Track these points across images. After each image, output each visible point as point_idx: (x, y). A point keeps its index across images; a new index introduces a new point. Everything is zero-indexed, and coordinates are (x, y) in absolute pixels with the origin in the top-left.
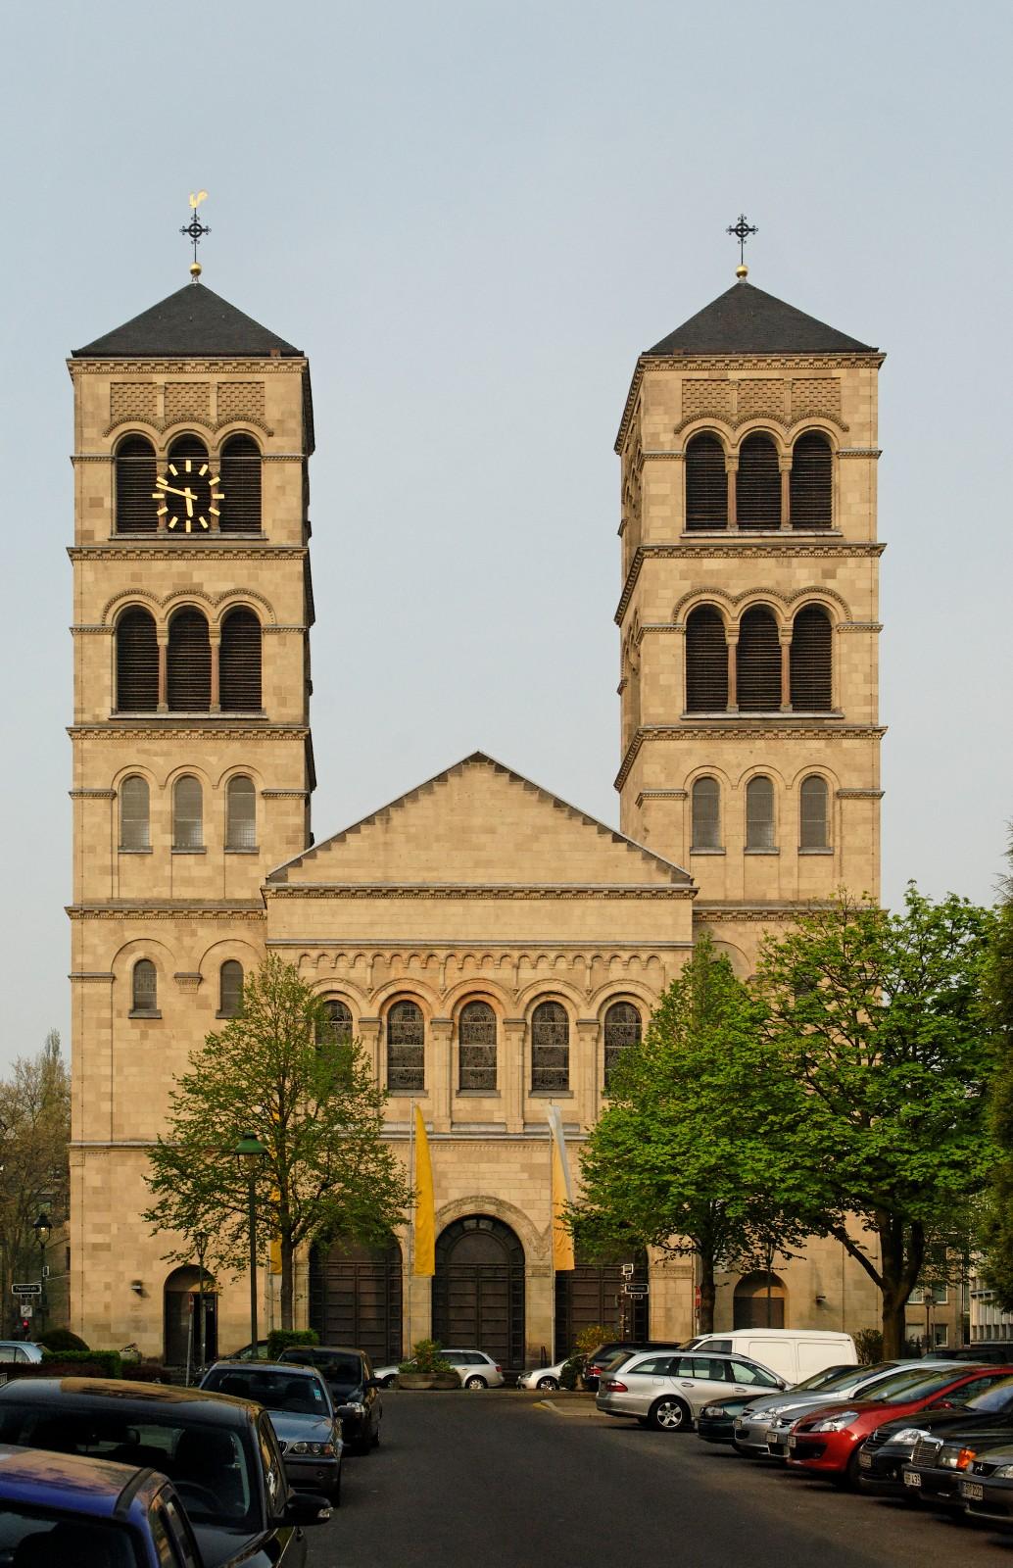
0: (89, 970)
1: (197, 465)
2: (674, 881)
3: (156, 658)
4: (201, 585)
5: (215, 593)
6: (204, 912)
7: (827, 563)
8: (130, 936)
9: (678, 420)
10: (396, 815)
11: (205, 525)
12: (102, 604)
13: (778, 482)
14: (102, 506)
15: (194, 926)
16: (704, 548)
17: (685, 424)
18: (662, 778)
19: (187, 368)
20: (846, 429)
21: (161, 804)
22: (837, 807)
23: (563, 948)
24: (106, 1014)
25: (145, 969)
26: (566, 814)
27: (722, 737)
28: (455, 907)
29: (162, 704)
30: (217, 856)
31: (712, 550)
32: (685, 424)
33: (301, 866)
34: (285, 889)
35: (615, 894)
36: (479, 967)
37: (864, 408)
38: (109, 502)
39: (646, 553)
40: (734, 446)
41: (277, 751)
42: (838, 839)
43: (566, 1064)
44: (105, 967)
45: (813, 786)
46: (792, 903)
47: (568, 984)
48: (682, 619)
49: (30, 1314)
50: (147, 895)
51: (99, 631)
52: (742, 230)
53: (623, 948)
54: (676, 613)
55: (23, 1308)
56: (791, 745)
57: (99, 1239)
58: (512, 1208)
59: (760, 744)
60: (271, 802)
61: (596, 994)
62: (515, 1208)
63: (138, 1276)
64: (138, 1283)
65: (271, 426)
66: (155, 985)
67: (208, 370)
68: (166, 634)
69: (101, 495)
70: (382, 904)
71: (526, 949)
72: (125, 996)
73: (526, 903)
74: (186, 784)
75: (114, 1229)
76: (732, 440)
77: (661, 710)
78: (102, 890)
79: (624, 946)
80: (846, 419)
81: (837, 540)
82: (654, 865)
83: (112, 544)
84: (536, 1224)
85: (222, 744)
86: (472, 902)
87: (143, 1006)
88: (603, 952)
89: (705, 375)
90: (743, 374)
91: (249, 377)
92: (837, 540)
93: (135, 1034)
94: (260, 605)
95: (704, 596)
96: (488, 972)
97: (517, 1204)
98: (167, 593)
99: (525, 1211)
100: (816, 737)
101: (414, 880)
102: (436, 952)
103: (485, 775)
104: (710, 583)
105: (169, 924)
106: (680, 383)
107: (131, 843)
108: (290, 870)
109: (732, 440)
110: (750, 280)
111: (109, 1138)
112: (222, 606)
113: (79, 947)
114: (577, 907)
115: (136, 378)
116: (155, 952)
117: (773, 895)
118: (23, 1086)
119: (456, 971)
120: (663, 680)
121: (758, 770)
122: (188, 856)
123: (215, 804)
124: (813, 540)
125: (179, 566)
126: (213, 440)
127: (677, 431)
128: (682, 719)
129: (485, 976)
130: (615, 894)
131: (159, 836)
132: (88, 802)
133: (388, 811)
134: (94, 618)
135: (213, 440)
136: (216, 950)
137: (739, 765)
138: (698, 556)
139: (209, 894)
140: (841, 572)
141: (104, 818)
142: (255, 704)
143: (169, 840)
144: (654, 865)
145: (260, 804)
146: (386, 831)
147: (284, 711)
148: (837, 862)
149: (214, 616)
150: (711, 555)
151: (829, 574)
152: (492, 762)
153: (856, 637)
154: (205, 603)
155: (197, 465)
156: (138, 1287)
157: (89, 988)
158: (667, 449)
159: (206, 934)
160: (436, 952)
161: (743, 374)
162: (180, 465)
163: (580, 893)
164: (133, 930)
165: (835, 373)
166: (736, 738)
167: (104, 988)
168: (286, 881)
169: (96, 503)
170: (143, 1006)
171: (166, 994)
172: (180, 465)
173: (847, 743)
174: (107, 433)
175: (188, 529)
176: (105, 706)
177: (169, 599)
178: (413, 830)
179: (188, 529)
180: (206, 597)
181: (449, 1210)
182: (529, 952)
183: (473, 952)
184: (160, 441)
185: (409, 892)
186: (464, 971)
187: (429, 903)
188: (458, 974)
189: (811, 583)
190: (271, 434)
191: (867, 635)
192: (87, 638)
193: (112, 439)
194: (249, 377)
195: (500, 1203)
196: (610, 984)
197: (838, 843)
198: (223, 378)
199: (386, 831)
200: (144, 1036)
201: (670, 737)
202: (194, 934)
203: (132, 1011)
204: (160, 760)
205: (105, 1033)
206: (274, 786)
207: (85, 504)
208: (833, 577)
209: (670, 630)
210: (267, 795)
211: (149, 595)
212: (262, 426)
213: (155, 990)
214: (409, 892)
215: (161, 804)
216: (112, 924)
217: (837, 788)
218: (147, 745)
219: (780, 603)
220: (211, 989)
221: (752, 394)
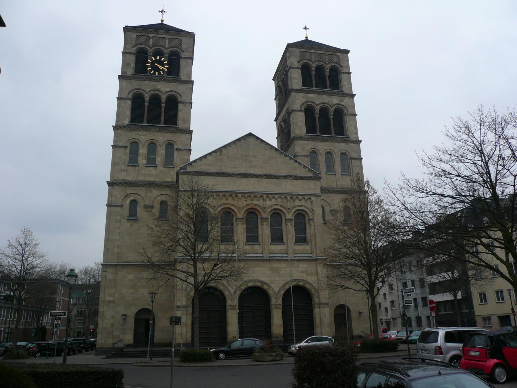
0: (113, 203)
1: (160, 58)
2: (313, 175)
3: (144, 109)
4: (160, 88)
5: (164, 91)
6: (155, 185)
7: (341, 98)
8: (129, 192)
9: (298, 60)
10: (224, 151)
11: (162, 73)
12: (128, 91)
13: (325, 77)
14: (130, 65)
15: (151, 189)
16: (308, 91)
17: (300, 61)
18: (301, 151)
19: (159, 33)
20: (342, 67)
21: (143, 151)
22: (350, 162)
23: (280, 195)
24: (118, 218)
25: (134, 203)
26: (279, 153)
27: (317, 141)
28: (244, 180)
29: (145, 121)
30: (160, 168)
31: (310, 91)
32: (300, 61)
33: (191, 165)
34: (186, 172)
35: (296, 178)
36: (252, 200)
37: (346, 62)
38: (133, 65)
39: (292, 91)
40: (313, 68)
41: (182, 137)
42: (351, 171)
43: (282, 234)
44: (119, 202)
45: (344, 154)
46: (341, 188)
47: (282, 206)
48: (303, 109)
49: (93, 328)
50: (136, 179)
51: (127, 99)
52: (306, 29)
53: (299, 195)
54: (301, 106)
55: (91, 326)
56: (336, 144)
57: (111, 299)
58: (266, 283)
59: (328, 143)
60: (179, 152)
61: (291, 209)
62: (267, 284)
63: (125, 313)
64: (125, 315)
65: (183, 50)
66: (137, 209)
67: (165, 34)
68: (148, 102)
69: (130, 63)
70: (219, 178)
71: (269, 195)
72: (126, 211)
73: (267, 180)
74: (152, 146)
75: (117, 295)
76: (314, 65)
77: (299, 132)
78: (122, 177)
79: (300, 194)
80: (342, 64)
81: (343, 93)
82: (307, 170)
83: (133, 76)
84: (274, 289)
85: (164, 134)
86: (250, 179)
87: (133, 214)
88: (293, 196)
89: (305, 50)
90: (315, 51)
91: (177, 37)
92: (343, 93)
93: (128, 225)
94: (178, 95)
95: (309, 103)
96: (255, 202)
97: (268, 282)
98: (149, 90)
99: (271, 285)
100: (343, 142)
101: (230, 171)
102: (238, 194)
103: (253, 140)
104: (310, 100)
105: (143, 189)
106: (299, 51)
107: (133, 160)
108: (188, 166)
109: (314, 65)
110: (309, 39)
111: (116, 261)
112: (166, 95)
113: (110, 195)
114: (284, 182)
115: (144, 34)
116: (138, 198)
117: (335, 186)
118: (96, 268)
119: (245, 201)
120: (299, 124)
121: (328, 150)
122: (150, 167)
123: (161, 152)
124: (337, 92)
125: (153, 83)
126: (167, 52)
127: (298, 62)
128: (305, 135)
129: (255, 203)
130: (296, 178)
131: (142, 161)
132: (118, 149)
133: (221, 152)
134: (125, 95)
135: (167, 52)
136: (159, 197)
137: (322, 149)
138: (306, 93)
139: (158, 180)
140: (345, 100)
141: (125, 154)
142: (176, 123)
143: (145, 162)
144: (307, 170)
145: (175, 153)
146: (221, 155)
147: (184, 125)
148: (352, 177)
149: (164, 98)
150: (310, 93)
151: (342, 101)
152: (255, 136)
153: (351, 117)
154: (161, 94)
155: (160, 58)
156: (125, 317)
157: (113, 209)
158: (296, 66)
159: (155, 192)
160: (238, 194)
161: (315, 51)
162: (156, 58)
163: (285, 177)
164: (130, 190)
165: (338, 54)
166: (321, 141)
167: (119, 209)
168: (186, 169)
169: (129, 64)
170: (133, 214)
171: (141, 212)
172: (156, 58)
173: (351, 144)
174: (133, 47)
175: (157, 74)
176: (127, 121)
177: (149, 91)
178: (229, 155)
179: (157, 74)
180: (161, 92)
181: (244, 285)
182: (269, 196)
183: (250, 195)
184: (150, 51)
185: (229, 175)
186: (247, 201)
187: (235, 178)
188: (245, 202)
189: (337, 102)
190: (183, 52)
191: (353, 117)
192: (122, 101)
193: (135, 49)
194: (177, 37)
195: (262, 282)
196: (296, 207)
197: (351, 172)
198: (170, 37)
199: (221, 155)
200: (132, 226)
201: (302, 140)
202: (151, 192)
203: (128, 217)
204: (143, 137)
205: (118, 225)
206: (180, 147)
207: (125, 64)
208: (343, 101)
209: (301, 111)
210: (178, 150)
211: (144, 91)
212: (181, 50)
213: (137, 210)
214: (229, 175)
215: (143, 151)
216: (123, 188)
217: (350, 157)
218: (139, 133)
219: (330, 107)
220: (156, 211)
221: (317, 56)
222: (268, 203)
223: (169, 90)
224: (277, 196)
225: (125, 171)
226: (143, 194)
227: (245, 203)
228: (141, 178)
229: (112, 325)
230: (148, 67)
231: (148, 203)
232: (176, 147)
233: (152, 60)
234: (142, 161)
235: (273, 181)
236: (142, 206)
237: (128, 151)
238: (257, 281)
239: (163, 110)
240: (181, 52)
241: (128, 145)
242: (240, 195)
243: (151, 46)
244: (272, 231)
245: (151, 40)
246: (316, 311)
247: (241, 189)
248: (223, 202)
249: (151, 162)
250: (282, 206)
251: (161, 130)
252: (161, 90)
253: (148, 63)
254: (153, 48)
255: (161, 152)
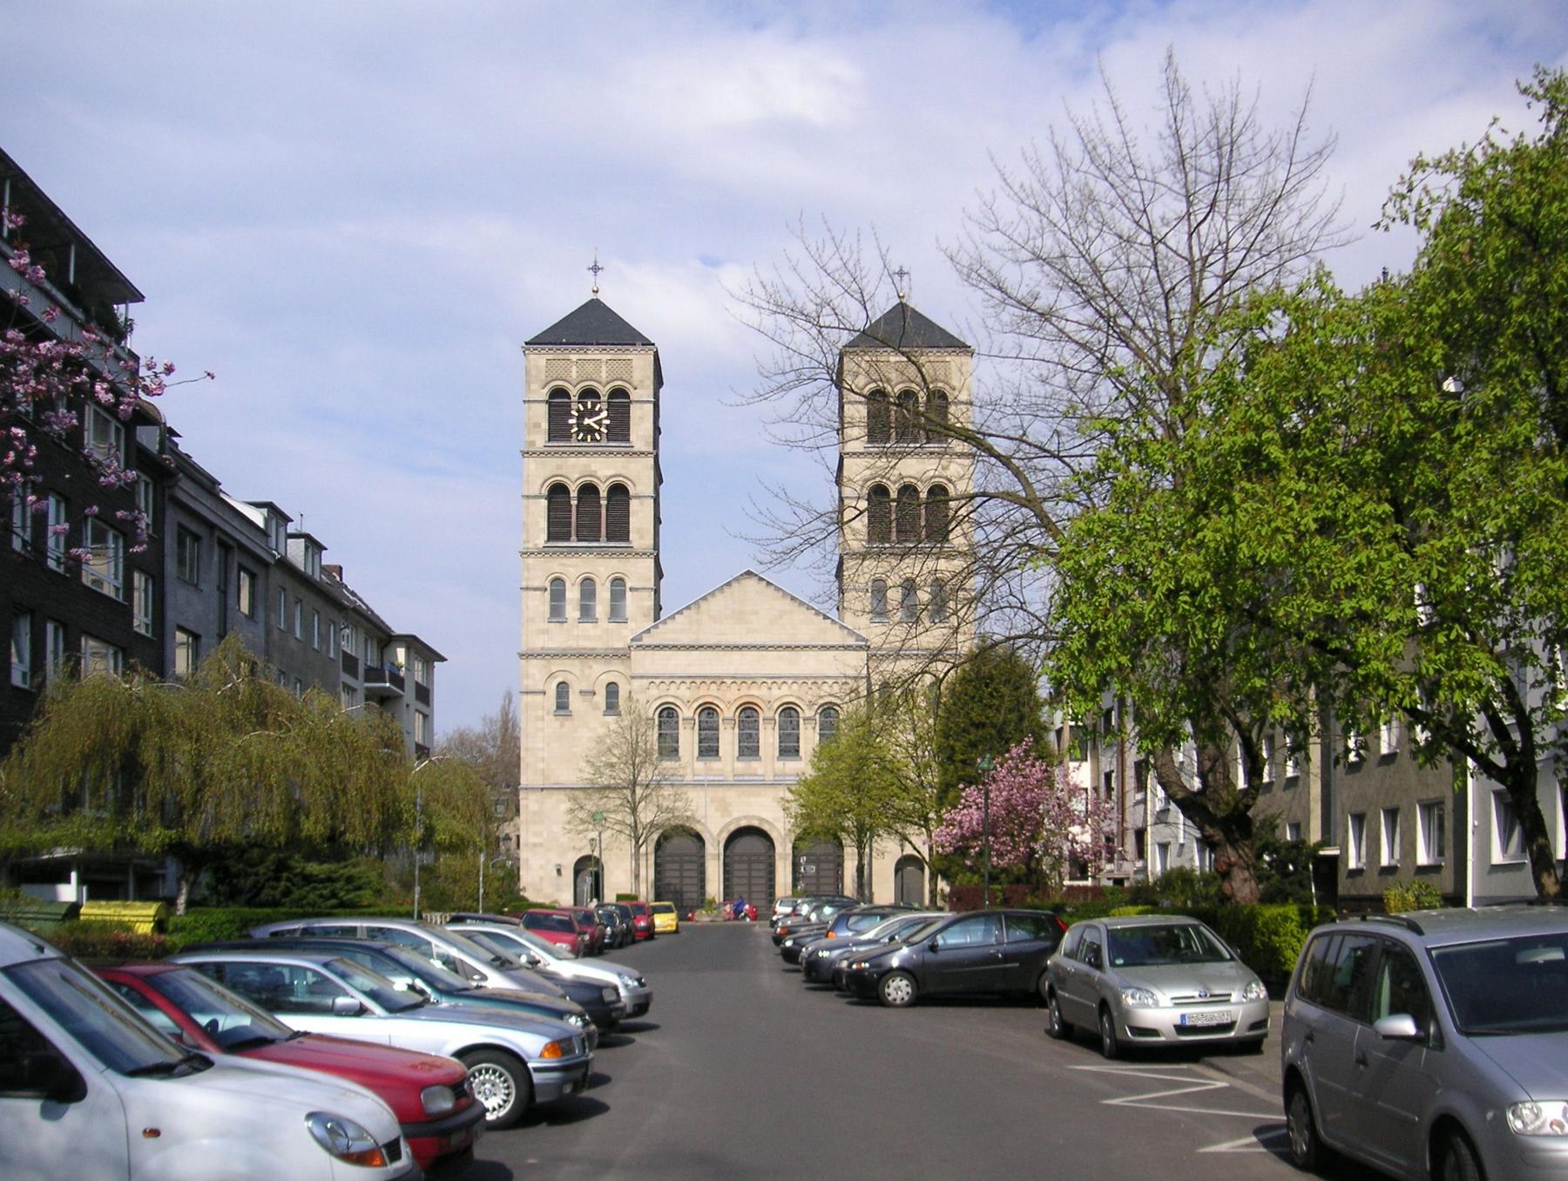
12: (540, 482)
21: (573, 594)
24: (540, 713)
25: (563, 688)
28: (736, 656)
29: (574, 537)
44: (540, 687)
47: (799, 698)
50: (564, 646)
63: (559, 862)
65: (635, 384)
70: (695, 653)
96: (754, 691)
114: (804, 654)
115: (561, 357)
116: (569, 678)
123: (603, 594)
125: (583, 460)
126: (604, 391)
131: (572, 611)
135: (604, 391)
143: (577, 614)
145: (628, 594)
159: (597, 667)
164: (556, 665)
167: (539, 698)
171: (574, 700)
172: (585, 405)
184: (574, 392)
193: (546, 390)
194: (624, 357)
195: (762, 820)
198: (609, 357)
200: (562, 725)
202: (591, 667)
204: (571, 569)
205: (540, 724)
215: (573, 594)
216: (543, 662)
218: (565, 561)
222: (776, 692)
223: (612, 472)
224: (790, 681)
225: (545, 632)
226: (577, 671)
227: (737, 694)
228: (573, 644)
229: (541, 879)
230: (571, 426)
231: (585, 687)
232: (629, 585)
233: (578, 411)
234: (572, 611)
235: (786, 654)
236: (577, 691)
237: (547, 594)
238: (754, 817)
239: (604, 511)
240: (631, 389)
241: (547, 585)
242: (729, 681)
243: (574, 382)
244: (782, 738)
245: (574, 369)
246: (522, 795)
247: (732, 671)
248: (701, 693)
249: (587, 612)
250: (799, 698)
251: (602, 553)
252: (599, 474)
253: (572, 416)
254: (579, 387)
255: (603, 594)
